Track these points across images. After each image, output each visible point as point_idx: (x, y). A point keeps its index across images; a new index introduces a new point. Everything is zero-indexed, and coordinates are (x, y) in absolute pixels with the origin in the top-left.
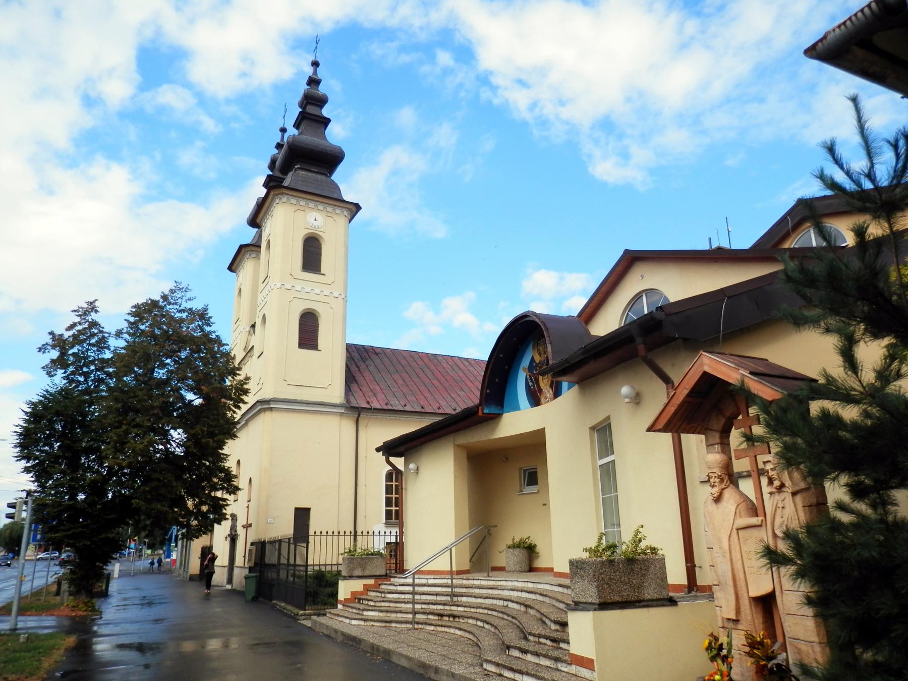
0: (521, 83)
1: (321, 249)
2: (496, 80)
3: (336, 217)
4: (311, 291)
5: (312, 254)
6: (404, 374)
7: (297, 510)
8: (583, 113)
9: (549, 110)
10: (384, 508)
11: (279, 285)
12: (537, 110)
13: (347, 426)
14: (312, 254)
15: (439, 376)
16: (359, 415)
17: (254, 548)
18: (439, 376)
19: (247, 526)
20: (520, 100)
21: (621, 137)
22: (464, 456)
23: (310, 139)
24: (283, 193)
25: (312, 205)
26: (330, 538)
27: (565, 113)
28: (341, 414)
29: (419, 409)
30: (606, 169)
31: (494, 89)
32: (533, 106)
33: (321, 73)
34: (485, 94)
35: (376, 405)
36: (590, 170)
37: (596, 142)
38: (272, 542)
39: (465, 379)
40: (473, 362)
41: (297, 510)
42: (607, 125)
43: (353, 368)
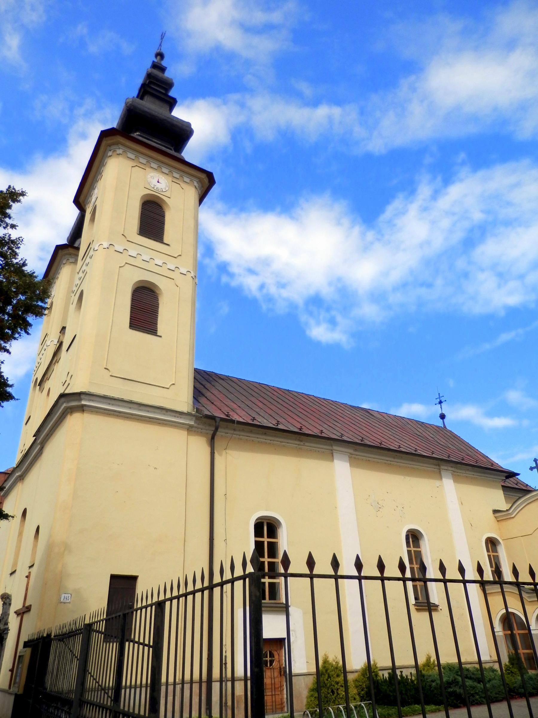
0: (251, 271)
1: (163, 217)
2: (234, 269)
3: (183, 185)
4: (149, 261)
5: (152, 219)
7: (114, 578)
8: (296, 294)
9: (273, 290)
11: (106, 245)
12: (265, 291)
13: (199, 446)
14: (152, 219)
16: (216, 429)
17: (29, 650)
19: (21, 613)
20: (251, 283)
21: (328, 309)
23: (150, 106)
24: (117, 144)
25: (154, 165)
27: (285, 293)
28: (190, 429)
30: (320, 332)
31: (231, 275)
32: (262, 287)
34: (224, 279)
36: (308, 333)
37: (311, 314)
38: (66, 636)
41: (114, 578)
42: (316, 302)
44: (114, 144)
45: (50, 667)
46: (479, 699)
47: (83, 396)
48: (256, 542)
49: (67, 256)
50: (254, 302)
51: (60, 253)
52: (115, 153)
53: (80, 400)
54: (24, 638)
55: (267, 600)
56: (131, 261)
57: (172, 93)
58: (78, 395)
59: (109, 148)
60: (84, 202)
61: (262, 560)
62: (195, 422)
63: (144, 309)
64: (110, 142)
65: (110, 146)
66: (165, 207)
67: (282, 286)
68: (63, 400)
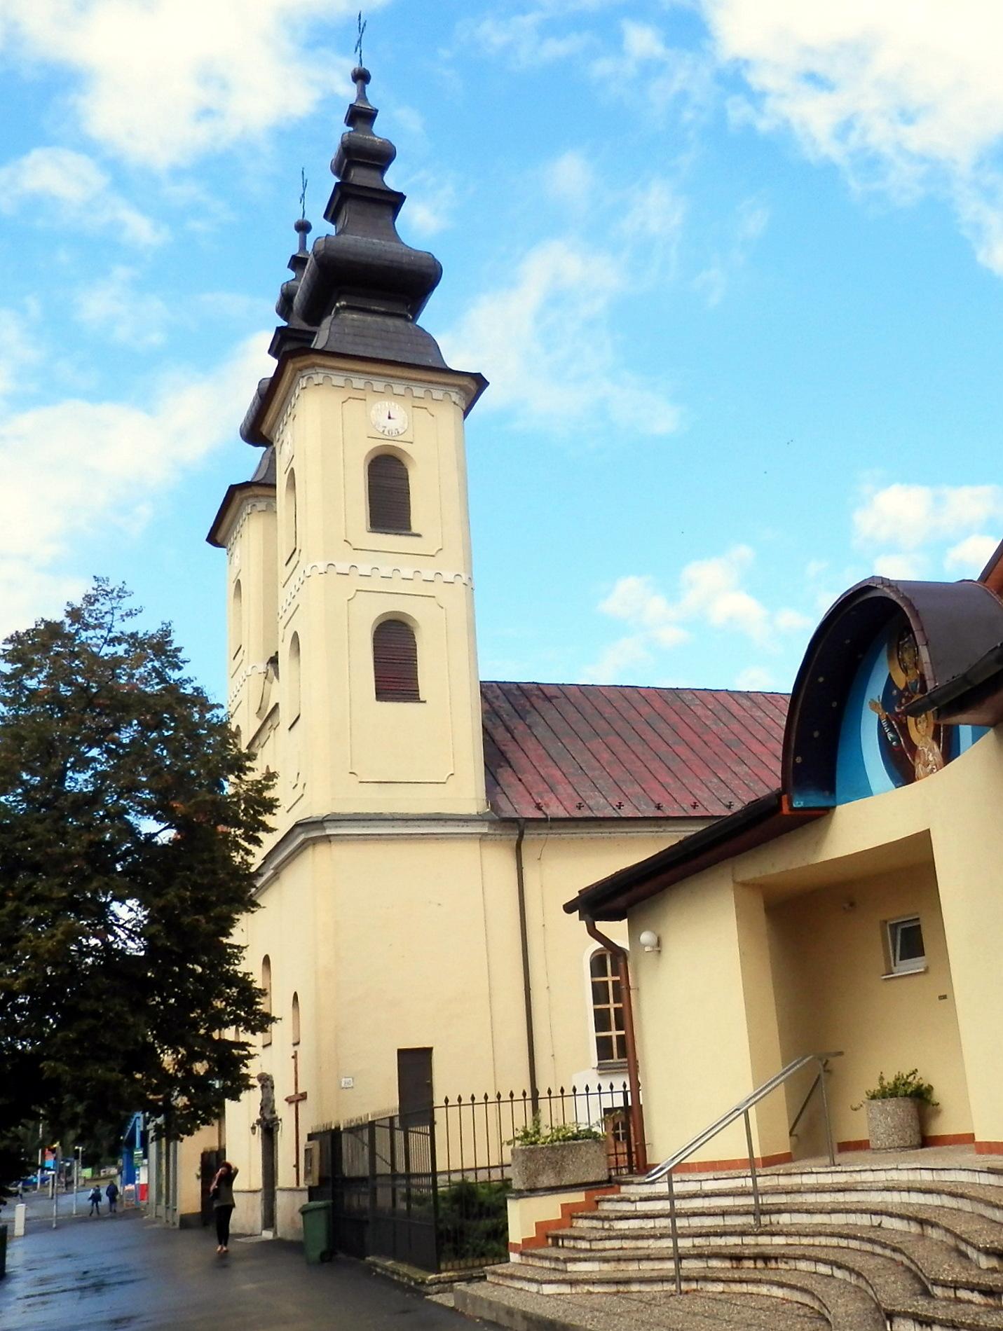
1: (406, 479)
5: (387, 494)
6: (612, 739)
9: (880, 135)
10: (592, 1035)
11: (322, 567)
12: (854, 138)
13: (498, 862)
14: (387, 494)
15: (689, 736)
16: (521, 835)
17: (315, 1145)
18: (689, 736)
19: (297, 1099)
22: (757, 905)
24: (313, 366)
26: (480, 1109)
27: (917, 138)
29: (651, 812)
32: (845, 129)
33: (376, 95)
35: (556, 810)
38: (354, 1130)
39: (745, 737)
40: (761, 699)
41: (402, 1053)
43: (500, 734)
44: (307, 367)
45: (344, 1157)
46: (45, 938)
47: (326, 824)
48: (595, 986)
49: (251, 501)
50: (829, 170)
51: (238, 496)
52: (311, 384)
53: (324, 829)
54: (304, 1132)
55: (616, 1059)
56: (365, 584)
57: (393, 179)
58: (319, 823)
59: (299, 374)
60: (269, 433)
61: (617, 1005)
62: (490, 828)
63: (395, 662)
64: (299, 365)
65: (300, 370)
66: (405, 461)
67: (907, 117)
68: (299, 830)
